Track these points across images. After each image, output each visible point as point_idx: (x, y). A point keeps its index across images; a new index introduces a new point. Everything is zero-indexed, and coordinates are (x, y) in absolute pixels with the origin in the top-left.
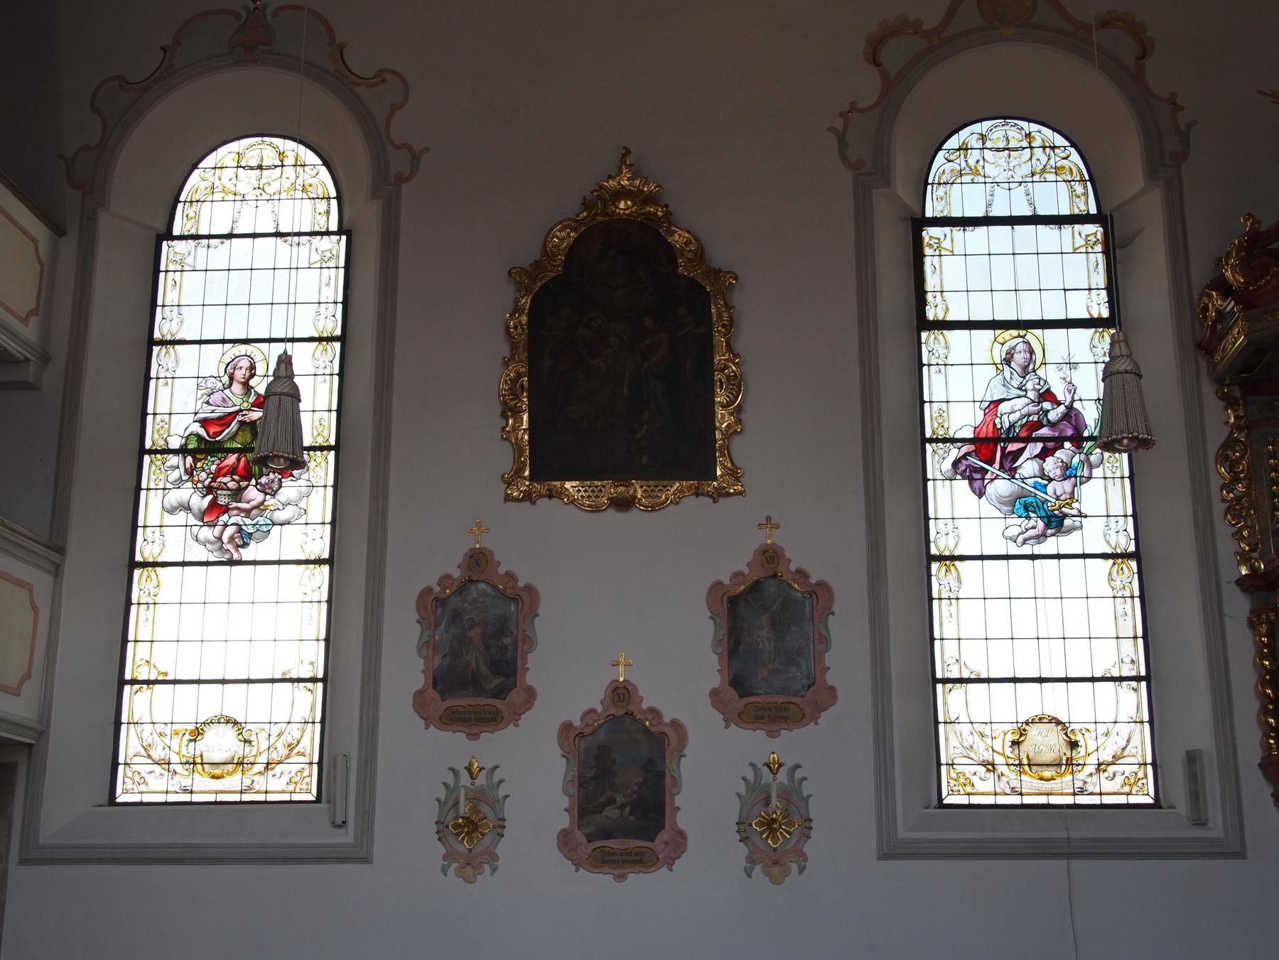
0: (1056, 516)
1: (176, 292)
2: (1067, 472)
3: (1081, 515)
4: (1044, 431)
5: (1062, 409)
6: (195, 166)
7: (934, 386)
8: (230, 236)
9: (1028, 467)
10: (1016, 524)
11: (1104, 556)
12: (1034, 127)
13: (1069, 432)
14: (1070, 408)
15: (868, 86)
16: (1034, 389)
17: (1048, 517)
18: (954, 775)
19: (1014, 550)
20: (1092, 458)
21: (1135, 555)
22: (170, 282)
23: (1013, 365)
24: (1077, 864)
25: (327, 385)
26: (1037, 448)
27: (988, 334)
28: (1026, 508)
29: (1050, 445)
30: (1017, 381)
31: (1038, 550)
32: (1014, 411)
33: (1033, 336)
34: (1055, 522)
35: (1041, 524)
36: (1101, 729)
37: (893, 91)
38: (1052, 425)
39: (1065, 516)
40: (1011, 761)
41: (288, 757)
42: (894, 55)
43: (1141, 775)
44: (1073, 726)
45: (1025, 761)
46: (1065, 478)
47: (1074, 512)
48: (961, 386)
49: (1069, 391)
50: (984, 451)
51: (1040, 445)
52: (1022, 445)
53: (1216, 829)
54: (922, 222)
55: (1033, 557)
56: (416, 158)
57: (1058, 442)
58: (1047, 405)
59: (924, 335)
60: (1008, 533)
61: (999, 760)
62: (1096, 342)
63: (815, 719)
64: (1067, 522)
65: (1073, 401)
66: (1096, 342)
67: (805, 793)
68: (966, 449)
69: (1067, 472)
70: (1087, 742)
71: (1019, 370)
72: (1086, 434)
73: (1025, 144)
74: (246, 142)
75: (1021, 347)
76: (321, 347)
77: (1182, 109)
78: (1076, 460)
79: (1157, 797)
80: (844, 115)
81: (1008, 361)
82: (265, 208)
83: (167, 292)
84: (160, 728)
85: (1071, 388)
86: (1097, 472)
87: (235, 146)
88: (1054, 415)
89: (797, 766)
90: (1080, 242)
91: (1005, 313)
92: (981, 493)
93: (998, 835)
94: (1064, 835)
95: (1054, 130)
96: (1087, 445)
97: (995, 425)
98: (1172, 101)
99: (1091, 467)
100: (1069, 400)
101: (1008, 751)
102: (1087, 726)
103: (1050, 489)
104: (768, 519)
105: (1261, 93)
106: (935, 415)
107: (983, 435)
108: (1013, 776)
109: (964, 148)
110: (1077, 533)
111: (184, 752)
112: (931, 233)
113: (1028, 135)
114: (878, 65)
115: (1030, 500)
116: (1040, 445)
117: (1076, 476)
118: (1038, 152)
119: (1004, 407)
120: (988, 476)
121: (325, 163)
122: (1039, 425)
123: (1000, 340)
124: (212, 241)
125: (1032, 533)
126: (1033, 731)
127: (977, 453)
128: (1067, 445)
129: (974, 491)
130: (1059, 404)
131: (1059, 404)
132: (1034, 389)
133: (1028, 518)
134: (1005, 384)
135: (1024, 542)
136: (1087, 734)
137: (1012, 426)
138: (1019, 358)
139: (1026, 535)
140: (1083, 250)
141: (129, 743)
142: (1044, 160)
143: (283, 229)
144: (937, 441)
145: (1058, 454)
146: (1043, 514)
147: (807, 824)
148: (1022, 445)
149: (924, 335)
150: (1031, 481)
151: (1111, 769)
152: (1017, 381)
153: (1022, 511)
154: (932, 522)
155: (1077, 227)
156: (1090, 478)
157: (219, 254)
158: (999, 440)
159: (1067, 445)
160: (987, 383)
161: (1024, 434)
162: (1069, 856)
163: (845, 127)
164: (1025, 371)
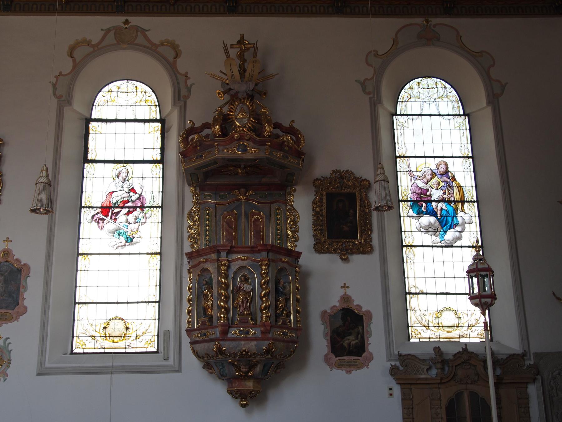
1: (402, 137)
4: (130, 204)
5: (137, 196)
6: (100, 91)
7: (88, 185)
8: (421, 115)
10: (115, 240)
12: (438, 80)
13: (139, 205)
14: (140, 195)
15: (67, 66)
17: (127, 238)
18: (78, 341)
21: (160, 253)
22: (399, 134)
24: (115, 376)
25: (469, 176)
26: (125, 211)
27: (112, 165)
28: (119, 235)
29: (131, 209)
30: (121, 184)
32: (117, 197)
33: (129, 166)
34: (130, 240)
35: (124, 241)
36: (139, 322)
37: (77, 68)
38: (133, 202)
39: (134, 238)
40: (102, 335)
41: (476, 324)
42: (79, 54)
43: (152, 340)
44: (128, 321)
45: (108, 335)
46: (136, 223)
48: (98, 186)
51: (127, 210)
53: (171, 362)
54: (89, 120)
56: (503, 87)
57: (135, 208)
58: (131, 194)
59: (86, 165)
61: (97, 335)
62: (153, 169)
63: (17, 319)
64: (134, 240)
66: (153, 169)
67: (10, 349)
70: (133, 327)
71: (122, 179)
72: (145, 206)
73: (435, 86)
74: (420, 79)
75: (125, 171)
76: (464, 161)
77: (190, 78)
79: (158, 349)
80: (57, 77)
82: (433, 105)
83: (399, 137)
84: (423, 312)
87: (116, 83)
88: (134, 198)
89: (7, 338)
90: (457, 125)
93: (85, 365)
94: (111, 364)
95: (446, 82)
96: (146, 210)
98: (186, 75)
100: (141, 192)
101: (101, 331)
102: (134, 321)
104: (8, 238)
106: (403, 191)
107: (105, 205)
108: (102, 341)
109: (110, 91)
111: (434, 322)
112: (92, 125)
113: (136, 87)
114: (72, 57)
115: (121, 231)
116: (127, 210)
118: (440, 90)
119: (114, 195)
120: (105, 222)
121: (153, 91)
124: (414, 117)
125: (120, 244)
126: (112, 323)
127: (102, 212)
128: (138, 209)
130: (136, 193)
131: (136, 193)
133: (119, 238)
136: (133, 324)
137: (117, 202)
138: (123, 175)
139: (117, 246)
140: (153, 133)
141: (412, 318)
142: (141, 96)
143: (442, 114)
144: (86, 207)
145: (134, 213)
147: (9, 362)
148: (119, 210)
149: (86, 165)
151: (141, 338)
152: (121, 184)
154: (403, 233)
155: (151, 124)
157: (418, 122)
158: (111, 207)
159: (138, 209)
161: (122, 205)
162: (112, 373)
163: (57, 81)
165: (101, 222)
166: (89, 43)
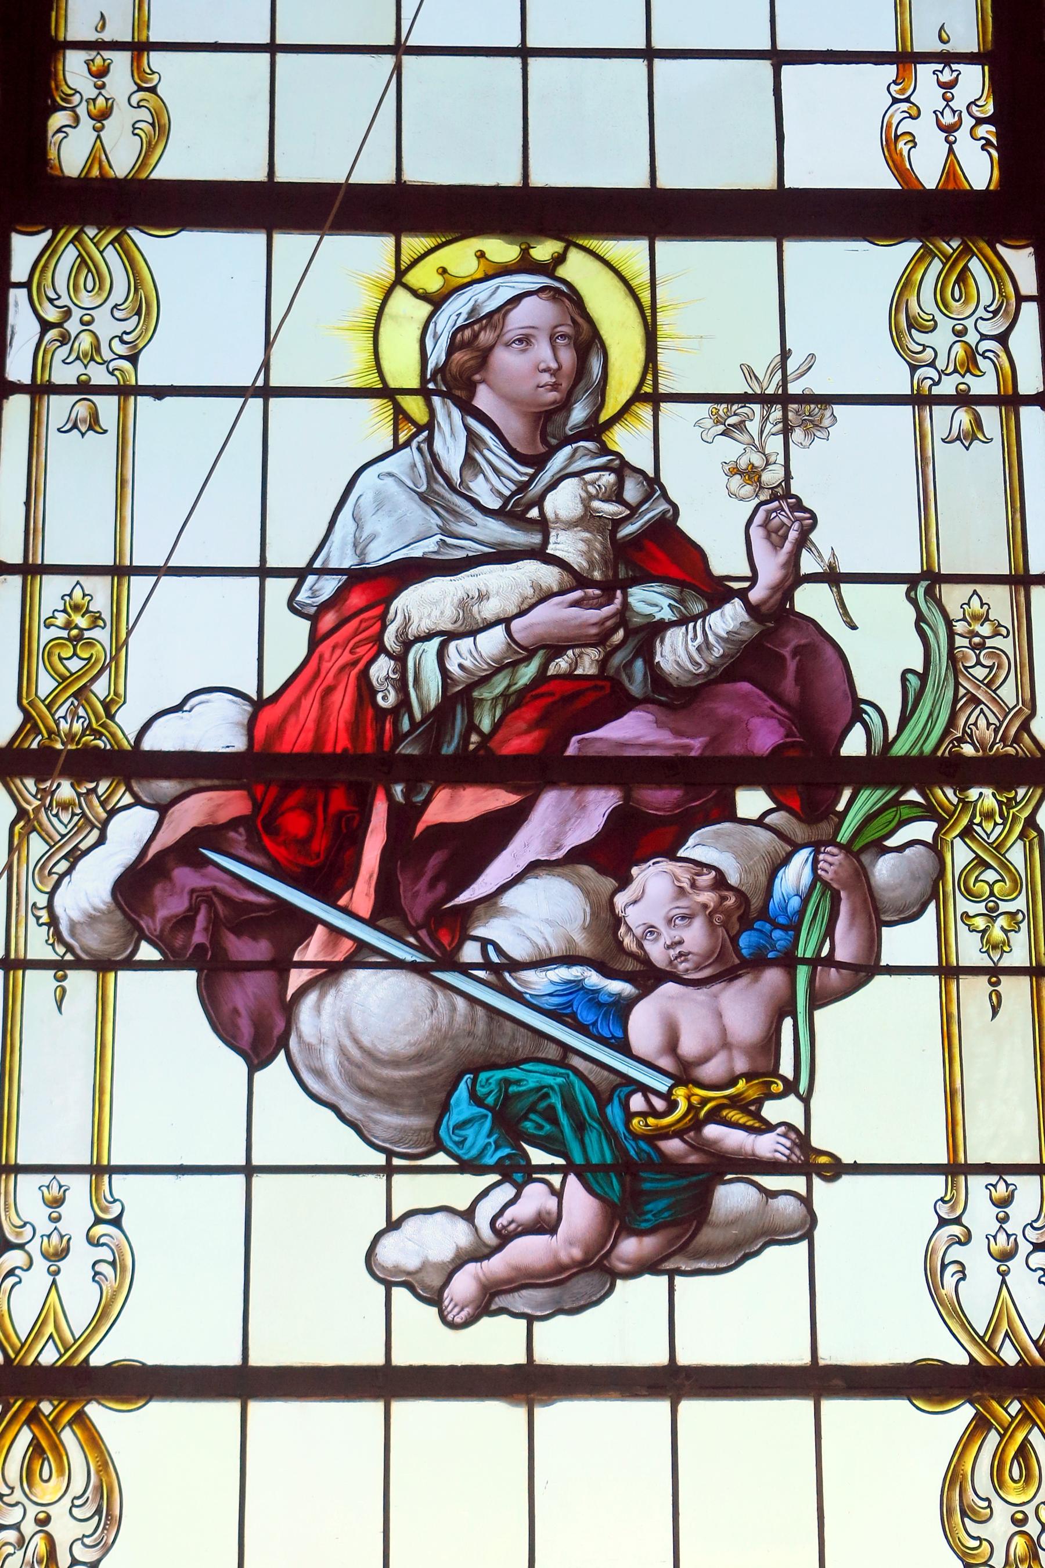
0: (669, 1165)
2: (746, 937)
3: (811, 1162)
4: (631, 730)
5: (728, 619)
9: (533, 912)
11: (920, 1382)
13: (765, 737)
16: (588, 520)
17: (625, 1167)
19: (423, 1339)
20: (884, 870)
23: (484, 399)
27: (370, 253)
28: (509, 1118)
29: (659, 799)
31: (565, 1341)
32: (477, 618)
34: (669, 1199)
35: (580, 1208)
38: (670, 697)
46: (727, 966)
47: (767, 1146)
49: (775, 536)
50: (296, 823)
51: (600, 805)
52: (501, 799)
55: (530, 1384)
57: (703, 789)
58: (650, 600)
60: (396, 1252)
65: (793, 578)
68: (195, 811)
69: (746, 937)
71: (513, 425)
72: (854, 745)
78: (796, 874)
81: (456, 379)
85: (784, 515)
86: (909, 942)
91: (460, 143)
92: (259, 1039)
96: (855, 806)
97: (366, 689)
99: (877, 915)
100: (770, 569)
103: (644, 1026)
105: (995, 1011)
107: (297, 738)
110: (783, 1261)
115: (531, 1077)
116: (600, 805)
117: (789, 962)
119: (424, 604)
120: (313, 949)
122: (608, 698)
123: (426, 278)
125: (529, 1251)
127: (259, 833)
129: (224, 1027)
130: (718, 592)
131: (718, 592)
132: (588, 520)
133: (516, 1172)
134: (438, 490)
135: (488, 1302)
137: (459, 696)
138: (524, 367)
139: (497, 1265)
145: (702, 846)
146: (598, 1151)
148: (501, 799)
150: (539, 982)
153: (479, 1138)
156: (868, 968)
158: (386, 766)
160: (329, 477)
161: (519, 742)
164: (547, 431)
165: (259, 949)
166: (84, 1544)
